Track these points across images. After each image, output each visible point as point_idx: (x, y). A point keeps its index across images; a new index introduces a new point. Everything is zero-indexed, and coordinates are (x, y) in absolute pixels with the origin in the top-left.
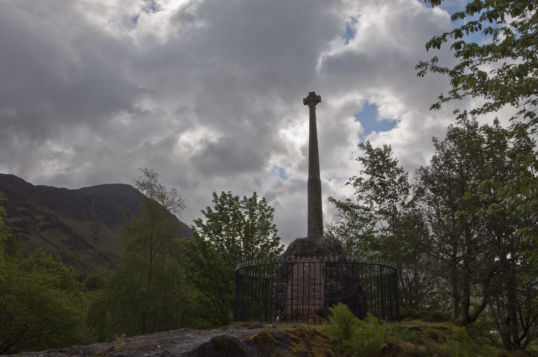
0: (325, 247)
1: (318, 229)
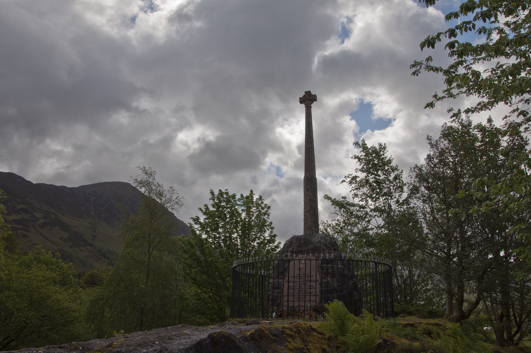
0: (320, 244)
1: (314, 226)
